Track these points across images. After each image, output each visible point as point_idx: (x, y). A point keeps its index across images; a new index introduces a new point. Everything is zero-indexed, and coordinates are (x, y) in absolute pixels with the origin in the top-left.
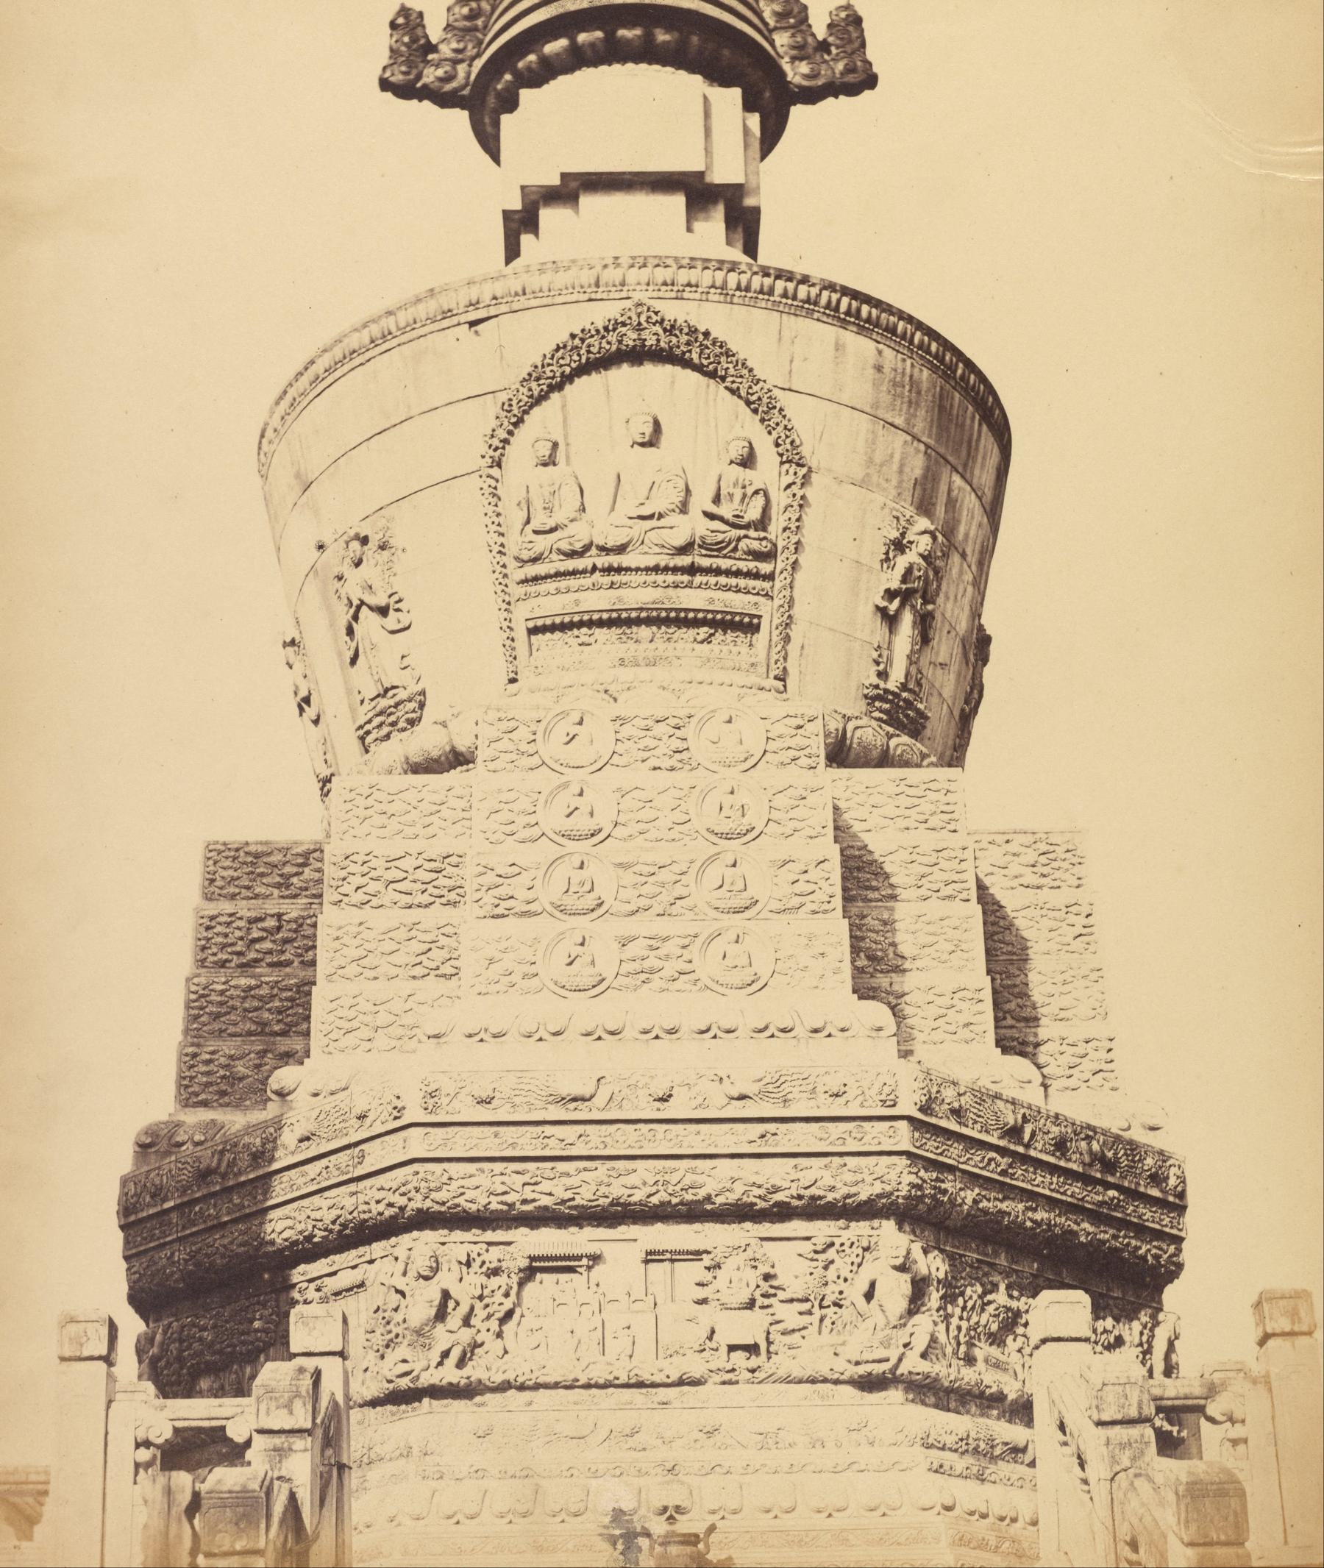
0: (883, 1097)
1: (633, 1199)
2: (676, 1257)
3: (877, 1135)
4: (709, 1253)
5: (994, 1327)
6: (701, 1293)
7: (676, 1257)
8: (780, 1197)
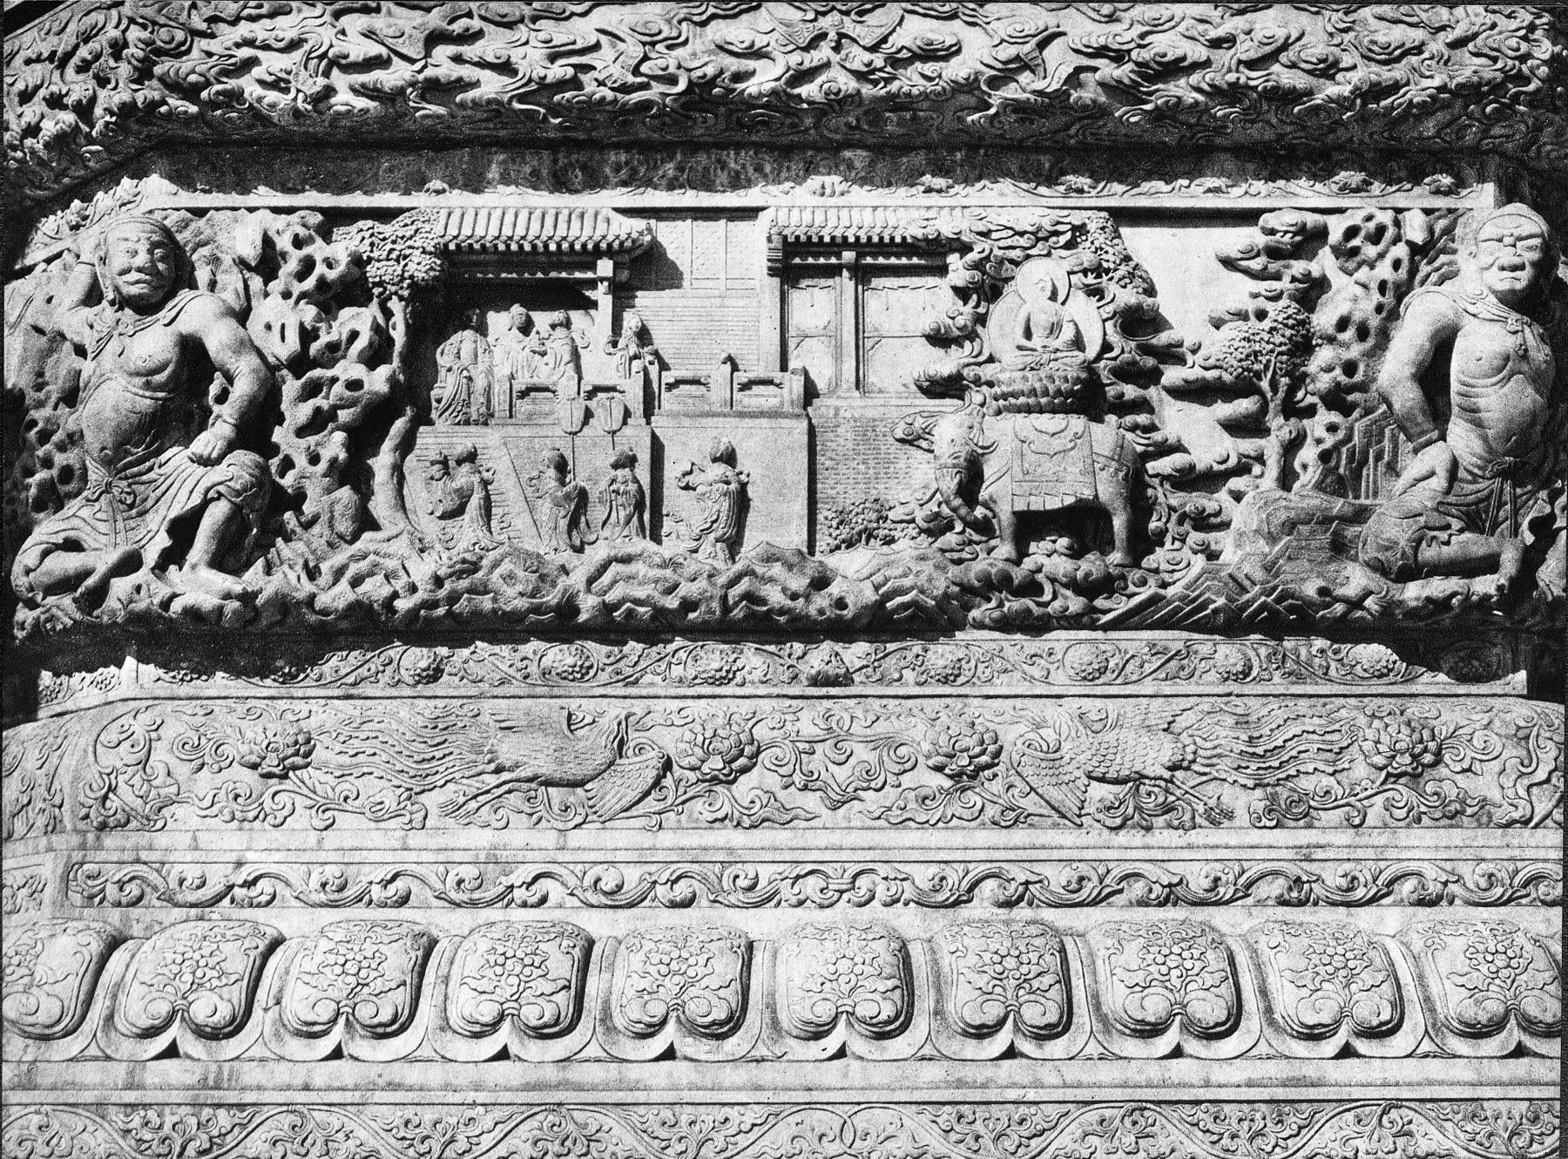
1: (751, 87)
2: (872, 260)
4: (965, 249)
6: (945, 363)
7: (872, 260)
8: (1181, 89)
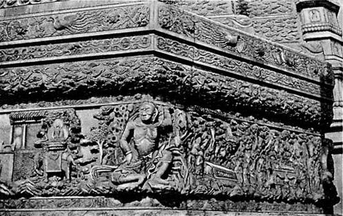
0: (140, 20)
3: (135, 44)
5: (223, 153)
6: (39, 141)
